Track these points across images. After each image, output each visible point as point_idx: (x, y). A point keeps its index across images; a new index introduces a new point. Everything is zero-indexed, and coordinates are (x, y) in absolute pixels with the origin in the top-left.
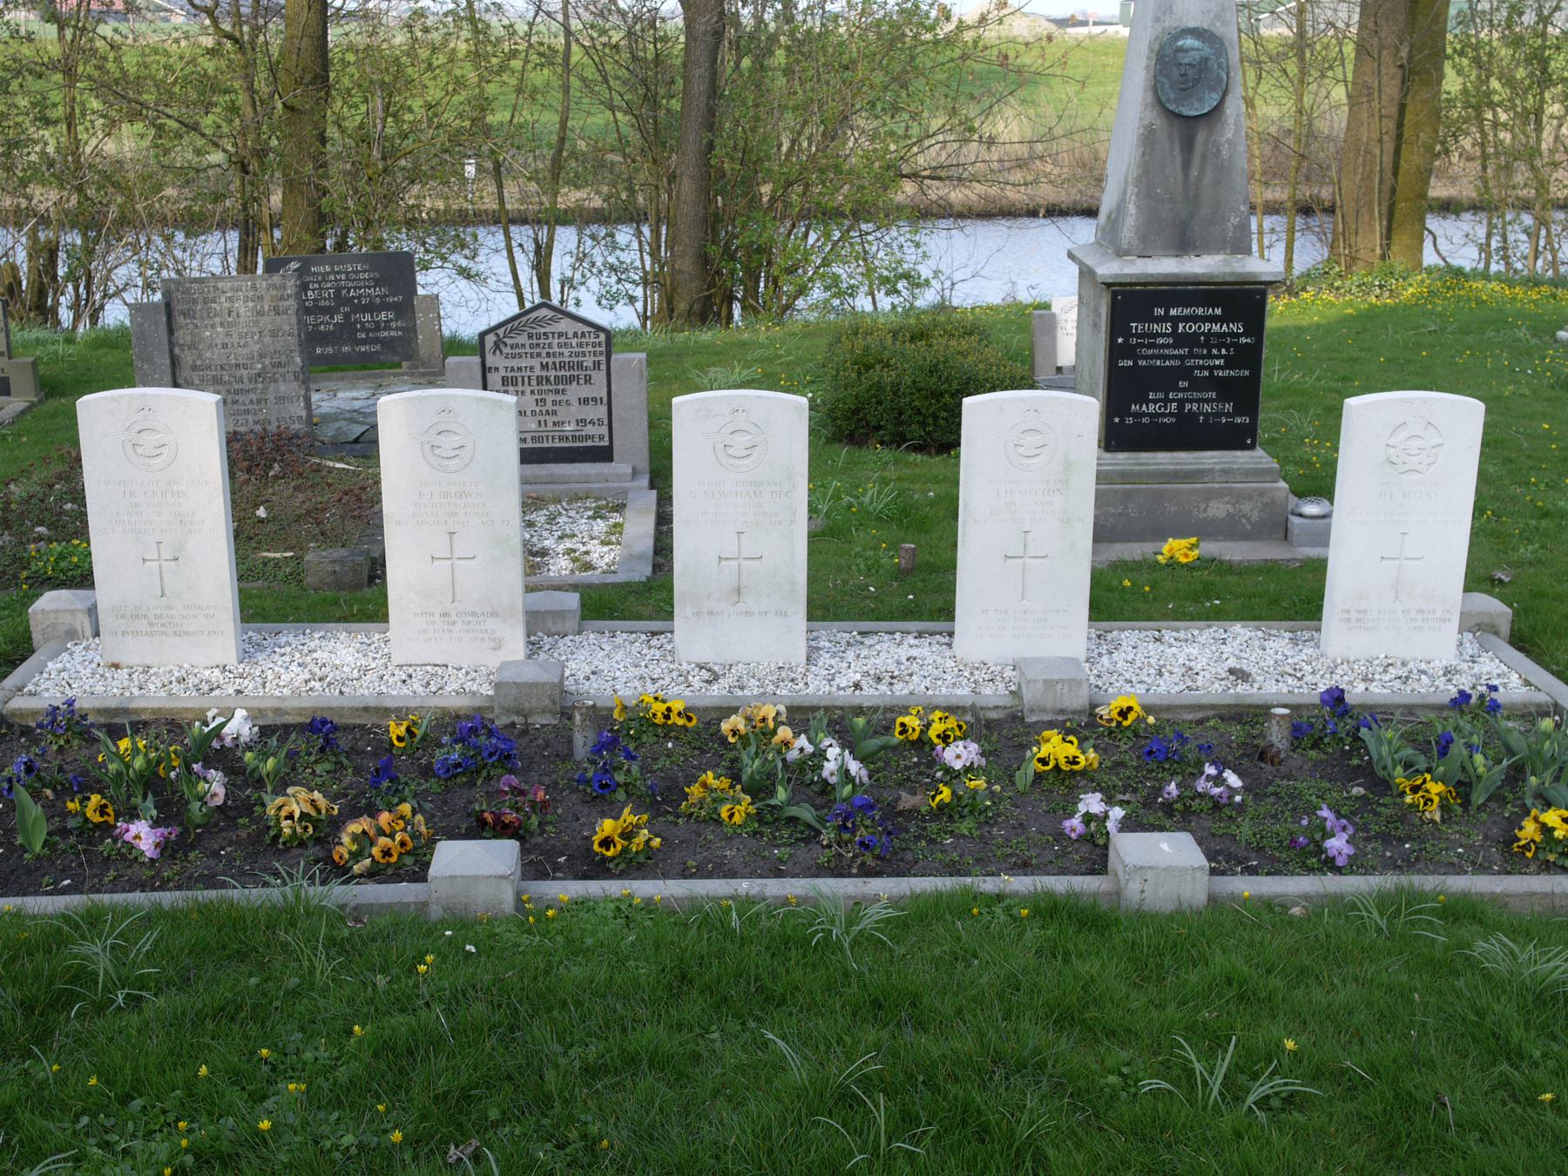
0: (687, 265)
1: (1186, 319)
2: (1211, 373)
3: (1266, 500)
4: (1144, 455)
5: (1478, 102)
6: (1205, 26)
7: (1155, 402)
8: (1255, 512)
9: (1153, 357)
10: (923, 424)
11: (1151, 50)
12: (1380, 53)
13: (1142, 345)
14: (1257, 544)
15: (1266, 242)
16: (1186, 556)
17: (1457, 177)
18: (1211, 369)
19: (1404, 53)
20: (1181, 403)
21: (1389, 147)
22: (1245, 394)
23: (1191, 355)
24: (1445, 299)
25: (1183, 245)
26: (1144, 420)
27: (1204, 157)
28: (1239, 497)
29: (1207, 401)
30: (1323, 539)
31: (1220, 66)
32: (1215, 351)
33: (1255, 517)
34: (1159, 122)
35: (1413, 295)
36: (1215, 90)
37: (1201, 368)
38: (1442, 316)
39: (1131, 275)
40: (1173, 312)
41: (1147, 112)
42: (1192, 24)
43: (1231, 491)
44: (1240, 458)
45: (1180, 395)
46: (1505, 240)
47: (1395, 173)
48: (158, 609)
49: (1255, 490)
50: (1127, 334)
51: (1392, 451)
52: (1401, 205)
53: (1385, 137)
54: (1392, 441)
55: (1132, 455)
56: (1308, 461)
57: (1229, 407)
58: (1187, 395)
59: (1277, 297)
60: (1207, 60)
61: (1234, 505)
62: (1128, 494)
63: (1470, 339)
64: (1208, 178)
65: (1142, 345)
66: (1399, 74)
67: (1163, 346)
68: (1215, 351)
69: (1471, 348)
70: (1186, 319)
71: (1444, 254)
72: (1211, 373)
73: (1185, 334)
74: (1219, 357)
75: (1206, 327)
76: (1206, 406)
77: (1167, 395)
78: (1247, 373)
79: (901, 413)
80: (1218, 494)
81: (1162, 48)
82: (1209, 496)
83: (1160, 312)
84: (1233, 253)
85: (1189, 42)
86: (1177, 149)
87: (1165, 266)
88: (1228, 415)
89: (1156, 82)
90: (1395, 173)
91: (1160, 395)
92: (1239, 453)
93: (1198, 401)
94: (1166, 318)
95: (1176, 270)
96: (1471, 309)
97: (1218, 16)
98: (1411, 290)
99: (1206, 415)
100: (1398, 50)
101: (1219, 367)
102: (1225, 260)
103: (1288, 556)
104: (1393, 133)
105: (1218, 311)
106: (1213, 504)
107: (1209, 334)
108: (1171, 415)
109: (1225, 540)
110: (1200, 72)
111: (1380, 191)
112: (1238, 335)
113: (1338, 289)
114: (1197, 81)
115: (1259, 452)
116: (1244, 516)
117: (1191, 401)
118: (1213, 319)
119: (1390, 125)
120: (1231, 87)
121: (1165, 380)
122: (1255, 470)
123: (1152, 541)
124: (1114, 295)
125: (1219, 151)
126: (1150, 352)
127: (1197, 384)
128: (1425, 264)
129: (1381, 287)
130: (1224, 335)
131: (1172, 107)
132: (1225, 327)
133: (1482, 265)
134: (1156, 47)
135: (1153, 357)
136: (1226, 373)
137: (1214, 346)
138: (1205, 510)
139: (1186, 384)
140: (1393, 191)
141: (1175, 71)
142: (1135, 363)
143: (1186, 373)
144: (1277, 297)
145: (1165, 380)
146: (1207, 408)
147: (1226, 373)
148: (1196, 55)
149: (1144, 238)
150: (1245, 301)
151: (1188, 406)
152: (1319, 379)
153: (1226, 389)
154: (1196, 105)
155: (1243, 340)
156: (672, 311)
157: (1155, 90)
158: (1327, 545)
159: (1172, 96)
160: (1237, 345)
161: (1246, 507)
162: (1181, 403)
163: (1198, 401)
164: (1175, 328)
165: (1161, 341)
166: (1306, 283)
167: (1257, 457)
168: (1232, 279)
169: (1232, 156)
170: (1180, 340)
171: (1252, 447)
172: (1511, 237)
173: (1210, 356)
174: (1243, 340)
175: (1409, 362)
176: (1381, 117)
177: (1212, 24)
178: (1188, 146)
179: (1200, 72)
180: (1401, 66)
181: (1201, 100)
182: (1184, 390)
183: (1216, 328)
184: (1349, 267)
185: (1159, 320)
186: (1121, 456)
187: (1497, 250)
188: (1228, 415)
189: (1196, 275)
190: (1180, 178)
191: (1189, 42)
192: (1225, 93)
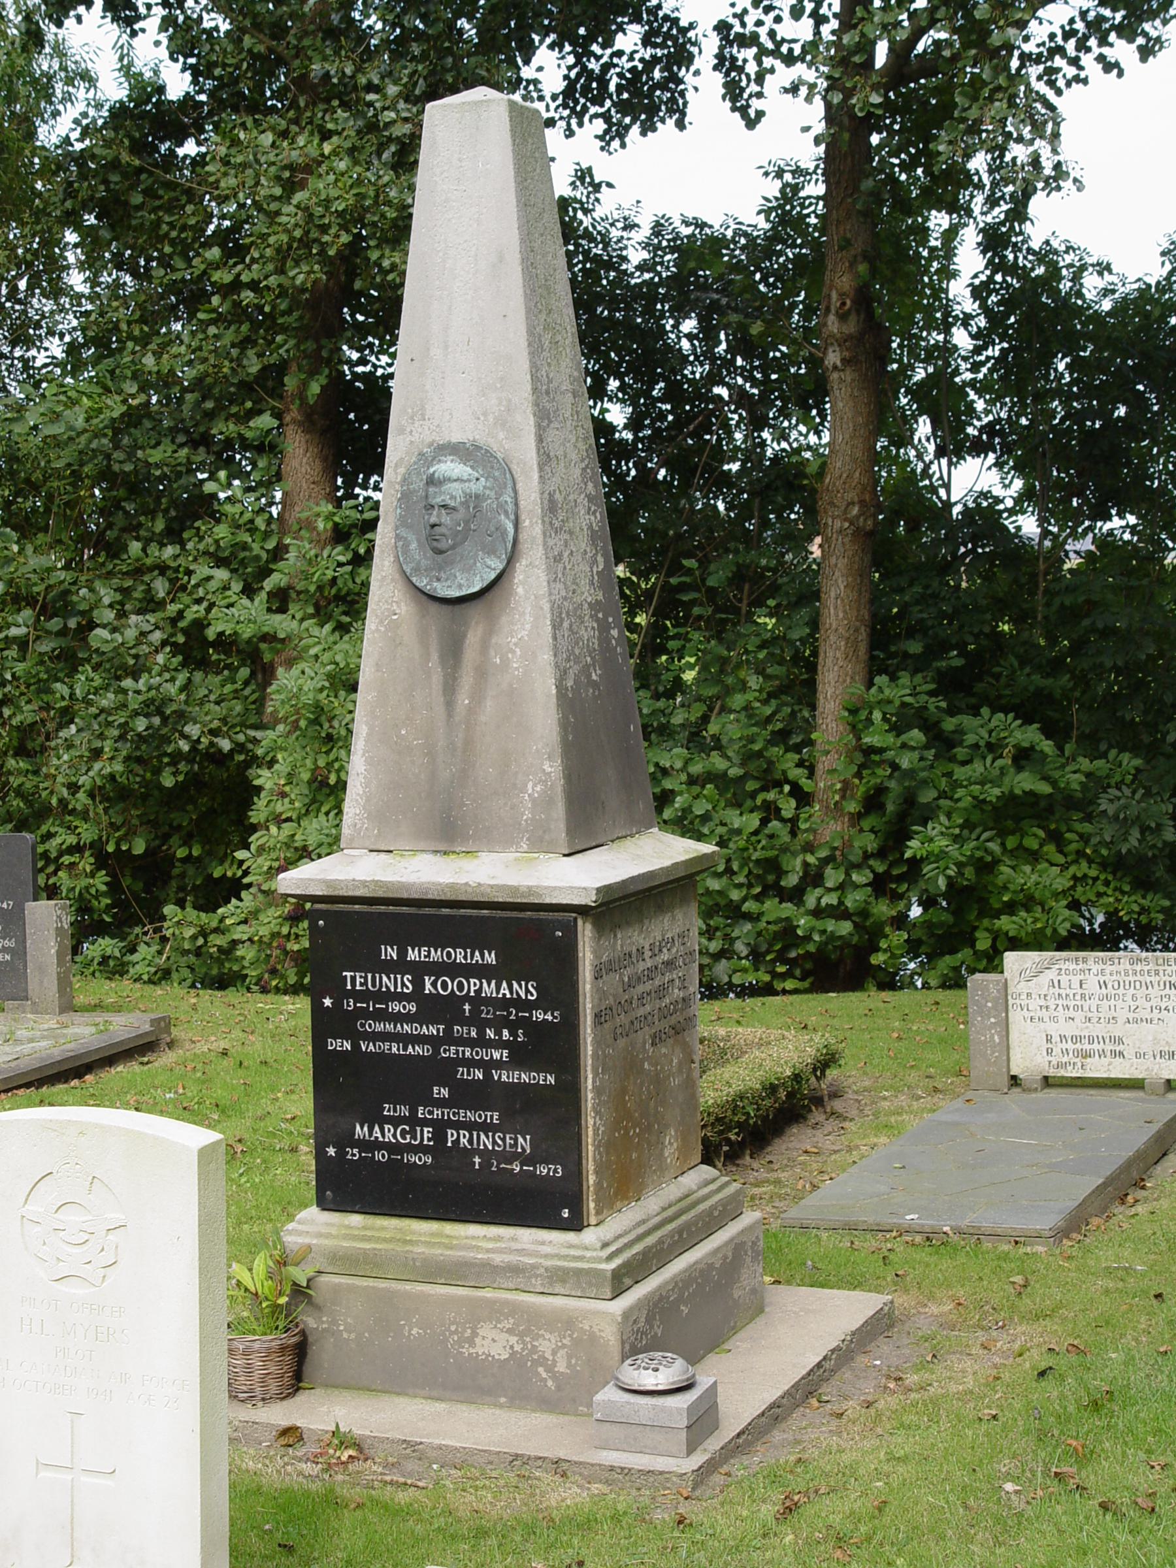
1: (437, 969)
2: (488, 1075)
7: (396, 1122)
13: (365, 1014)
18: (488, 1066)
20: (440, 1128)
23: (449, 1039)
26: (378, 1156)
28: (529, 1323)
29: (486, 1127)
31: (501, 506)
36: (491, 552)
37: (471, 1063)
40: (412, 955)
42: (456, 437)
43: (514, 1309)
45: (437, 1113)
48: (442, 1027)
57: (524, 1143)
58: (448, 1114)
61: (521, 1335)
65: (365, 1014)
67: (398, 1018)
68: (490, 1033)
70: (437, 969)
72: (488, 1075)
74: (500, 1044)
76: (489, 1141)
77: (414, 1111)
78: (551, 1079)
80: (495, 1312)
83: (390, 953)
86: (435, 656)
88: (527, 1160)
91: (404, 1111)
93: (470, 1126)
94: (400, 966)
99: (485, 1154)
101: (499, 1065)
105: (491, 958)
106: (486, 1330)
107: (478, 1000)
108: (421, 1149)
117: (458, 1126)
121: (409, 1081)
126: (379, 1027)
130: (505, 1003)
131: (422, 582)
132: (505, 990)
142: (356, 1046)
143: (444, 1071)
145: (409, 1081)
146: (486, 1141)
153: (519, 1106)
154: (461, 578)
155: (539, 1015)
160: (527, 1023)
162: (440, 1128)
163: (470, 1126)
164: (418, 984)
165: (395, 1007)
170: (435, 1008)
174: (539, 1015)
178: (452, 651)
182: (441, 1103)
185: (390, 967)
191: (449, 467)
192: (511, 561)
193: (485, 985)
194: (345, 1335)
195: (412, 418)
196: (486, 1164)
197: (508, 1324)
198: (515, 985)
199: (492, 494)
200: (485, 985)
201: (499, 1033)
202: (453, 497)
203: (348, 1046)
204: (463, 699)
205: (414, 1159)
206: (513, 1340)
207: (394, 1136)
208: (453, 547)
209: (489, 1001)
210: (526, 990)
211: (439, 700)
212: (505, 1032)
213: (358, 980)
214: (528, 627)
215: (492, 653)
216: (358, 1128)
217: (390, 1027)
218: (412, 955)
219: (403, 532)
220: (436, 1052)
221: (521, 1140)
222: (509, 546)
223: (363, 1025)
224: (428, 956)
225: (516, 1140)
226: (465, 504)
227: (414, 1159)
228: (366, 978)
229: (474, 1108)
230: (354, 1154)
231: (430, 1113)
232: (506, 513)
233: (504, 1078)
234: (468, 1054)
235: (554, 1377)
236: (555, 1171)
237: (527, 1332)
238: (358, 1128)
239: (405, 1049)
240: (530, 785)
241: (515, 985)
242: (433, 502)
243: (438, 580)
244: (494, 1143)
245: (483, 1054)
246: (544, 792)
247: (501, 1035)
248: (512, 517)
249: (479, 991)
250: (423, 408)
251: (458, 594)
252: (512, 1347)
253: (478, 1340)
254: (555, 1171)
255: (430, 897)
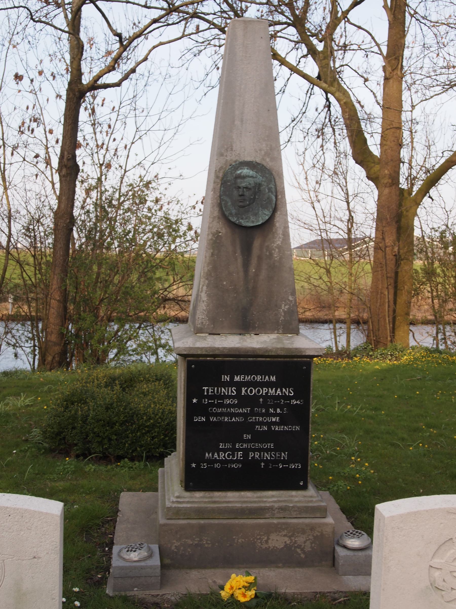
0: (53, 338)
1: (247, 384)
2: (269, 428)
3: (316, 533)
4: (217, 494)
5: (430, 273)
6: (258, 160)
7: (225, 451)
8: (308, 543)
9: (222, 414)
10: (101, 443)
11: (217, 177)
12: (385, 249)
13: (213, 405)
14: (308, 571)
15: (338, 334)
16: (244, 595)
17: (422, 308)
18: (269, 424)
19: (396, 249)
20: (246, 452)
21: (392, 291)
22: (298, 447)
23: (253, 414)
24: (422, 362)
25: (245, 326)
26: (216, 466)
27: (260, 258)
28: (294, 531)
30: (364, 569)
31: (270, 190)
32: (271, 411)
33: (308, 548)
34: (224, 230)
35: (406, 359)
38: (422, 370)
39: (202, 349)
40: (237, 379)
41: (215, 223)
44: (295, 497)
45: (245, 446)
46: (444, 334)
47: (395, 303)
49: (307, 525)
50: (201, 396)
51: (437, 574)
52: (398, 318)
53: (390, 287)
54: (437, 562)
55: (207, 494)
56: (354, 477)
59: (342, 359)
60: (260, 185)
61: (290, 537)
62: (202, 528)
63: (440, 384)
64: (263, 274)
65: (213, 405)
66: (394, 258)
67: (229, 406)
68: (271, 411)
69: (441, 389)
70: (247, 384)
71: (418, 341)
72: (269, 428)
73: (246, 396)
75: (264, 391)
76: (265, 454)
77: (234, 445)
78: (298, 428)
79: (87, 436)
80: (277, 528)
81: (225, 175)
82: (270, 529)
84: (284, 333)
85: (245, 171)
86: (239, 251)
87: (230, 342)
89: (221, 200)
90: (395, 303)
91: (229, 446)
92: (294, 493)
93: (260, 450)
94: (231, 383)
95: (238, 345)
96: (435, 367)
97: (267, 154)
98: (405, 357)
99: (267, 462)
100: (393, 248)
101: (275, 423)
102: (278, 338)
103: (335, 587)
104: (393, 285)
105: (273, 379)
106: (273, 537)
108: (237, 461)
109: (283, 567)
110: (255, 194)
111: (388, 311)
112: (290, 398)
113: (371, 356)
114: (253, 200)
115: (311, 491)
116: (299, 547)
117: (254, 450)
118: (269, 385)
119: (392, 281)
120: (279, 206)
121: (233, 433)
122: (307, 507)
123: (224, 567)
124: (189, 364)
125: (271, 255)
126: (220, 410)
127: (259, 437)
128: (410, 345)
129: (391, 355)
131: (234, 219)
132: (279, 392)
133: (435, 346)
134: (221, 175)
135: (222, 414)
136: (281, 428)
137: (271, 406)
138: (267, 542)
139: (249, 437)
140: (394, 311)
141: (235, 193)
142: (208, 419)
143: (248, 427)
144: (342, 359)
145: (233, 433)
146: (267, 456)
147: (281, 428)
148: (251, 181)
149: (213, 320)
150: (294, 370)
151: (251, 455)
152: (361, 409)
154: (252, 218)
155: (294, 402)
156: (45, 360)
157: (220, 206)
158: (368, 573)
159: (234, 211)
161: (300, 539)
163: (260, 450)
164: (239, 391)
166: (356, 352)
167: (310, 496)
168: (283, 353)
169: (281, 258)
170: (244, 401)
171: (305, 488)
172: (447, 334)
173: (268, 414)
174: (294, 402)
175: (410, 398)
176: (387, 277)
177: (263, 159)
178: (247, 250)
179: (255, 194)
180: (395, 255)
181: (256, 215)
182: (248, 441)
183: (272, 392)
184: (376, 346)
186: (198, 495)
187: (442, 339)
188: (284, 462)
189: (254, 350)
190: (241, 274)
191: (245, 171)
192: (275, 210)
193: (270, 390)
194: (206, 546)
195: (227, 150)
196: (266, 465)
197: (284, 533)
198: (284, 390)
199: (265, 184)
200: (270, 390)
201: (275, 410)
202: (250, 184)
203: (204, 419)
204: (253, 270)
205: (234, 466)
206: (286, 539)
207: (224, 457)
208: (249, 205)
209: (273, 397)
210: (289, 392)
211: (241, 269)
212: (278, 410)
213: (210, 390)
214: (281, 240)
215: (265, 250)
216: (207, 454)
217: (224, 410)
218: (237, 379)
219: (224, 197)
220: (246, 420)
221: (283, 454)
222: (274, 206)
223: (211, 410)
224: (244, 379)
225: (281, 454)
226: (254, 187)
227: (234, 466)
228: (214, 390)
229: (262, 442)
230: (205, 466)
231: (242, 446)
232: (272, 192)
233: (277, 429)
234: (261, 419)
235: (304, 553)
236: (298, 466)
237: (292, 536)
238: (207, 454)
239: (231, 419)
240: (283, 305)
241: (284, 390)
242: (240, 185)
243: (242, 219)
244: (271, 456)
245: (268, 420)
246: (289, 309)
247: (276, 411)
248: (275, 194)
249: (267, 393)
250: (232, 146)
251: (252, 225)
252: (285, 542)
253: (270, 541)
254: (298, 466)
255: (249, 353)
